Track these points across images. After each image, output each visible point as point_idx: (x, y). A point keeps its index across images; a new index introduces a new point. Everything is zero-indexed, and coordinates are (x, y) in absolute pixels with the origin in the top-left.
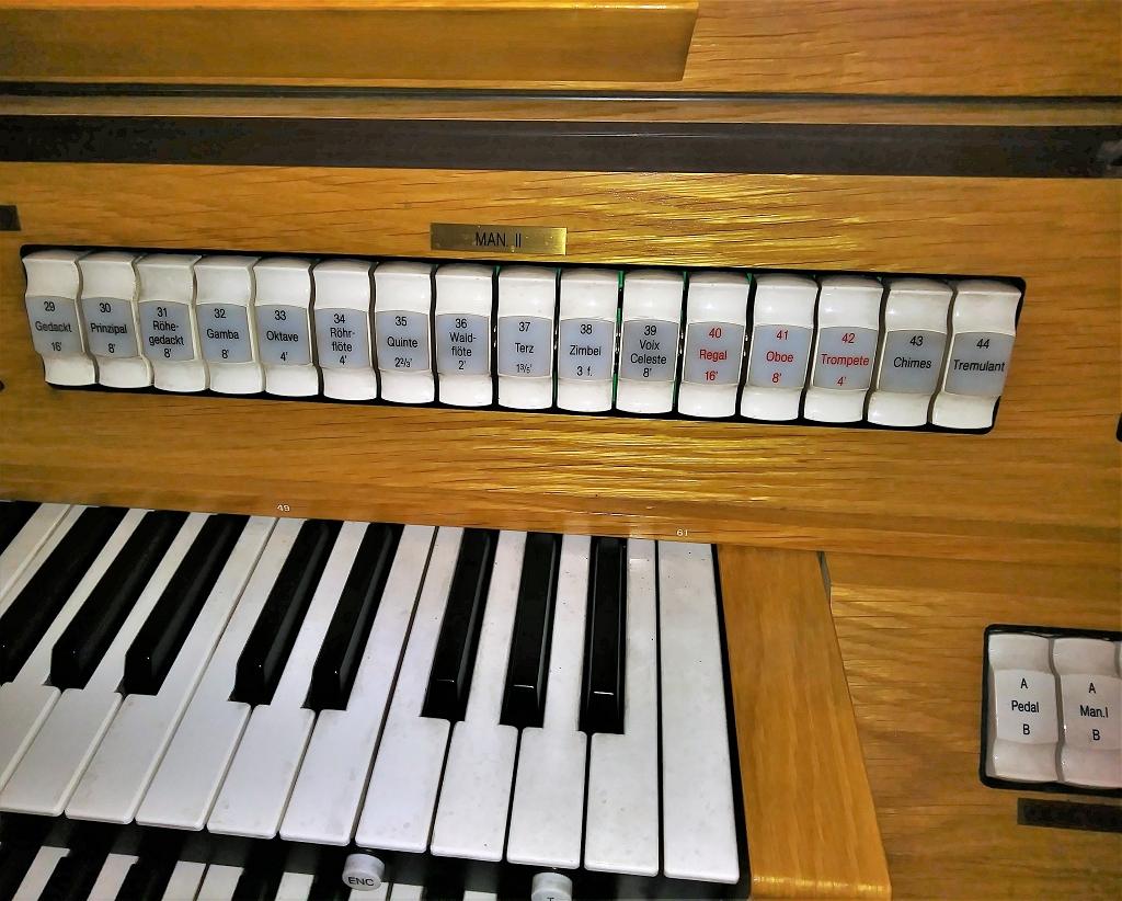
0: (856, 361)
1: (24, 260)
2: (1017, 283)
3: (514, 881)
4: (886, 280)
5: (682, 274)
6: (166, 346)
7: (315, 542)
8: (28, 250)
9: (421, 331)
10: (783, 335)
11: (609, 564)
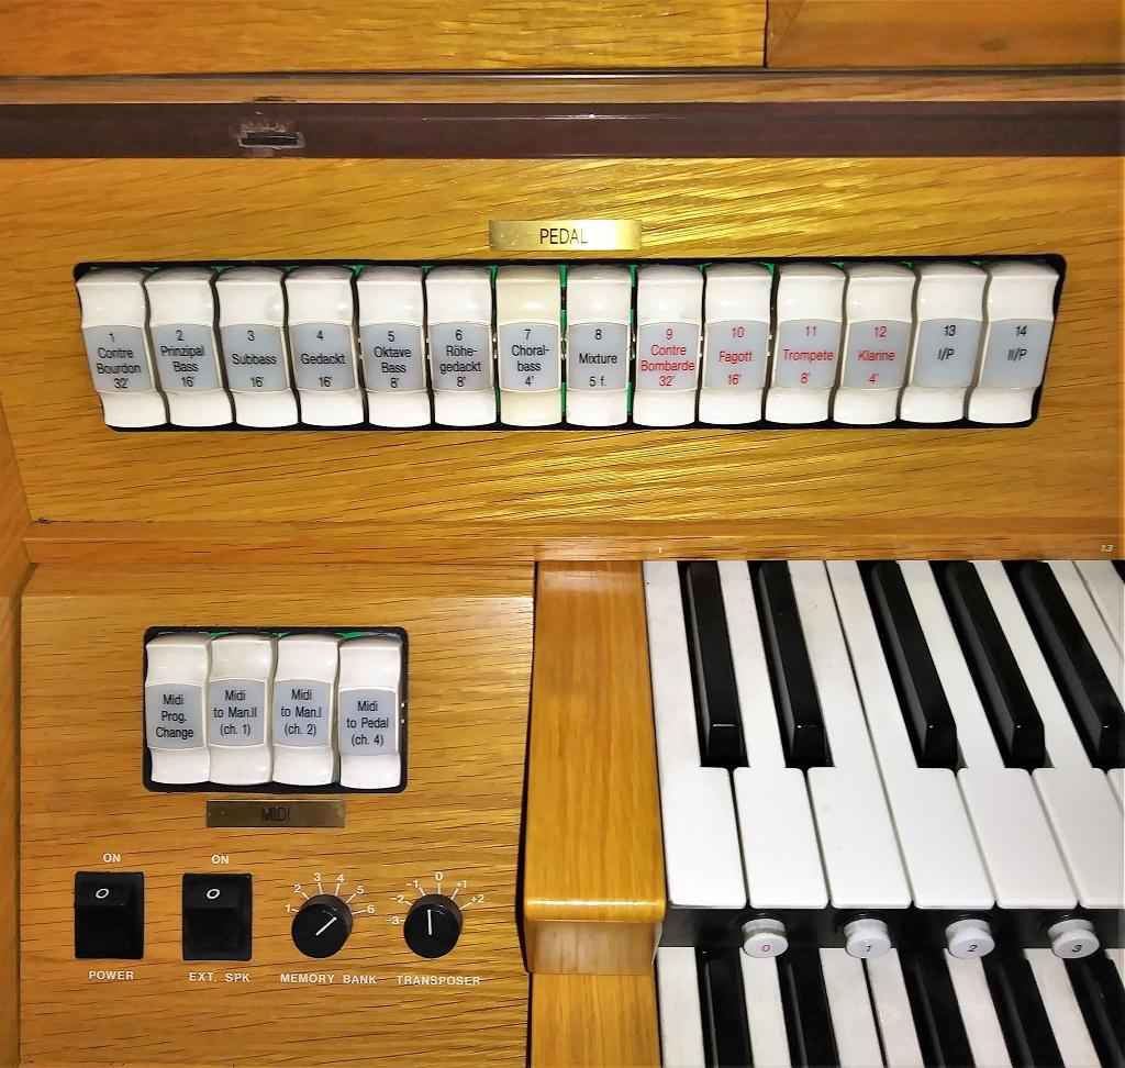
0: (819, 356)
1: (80, 284)
2: (1055, 263)
4: (776, 266)
6: (460, 374)
7: (700, 587)
10: (812, 330)
11: (1034, 582)
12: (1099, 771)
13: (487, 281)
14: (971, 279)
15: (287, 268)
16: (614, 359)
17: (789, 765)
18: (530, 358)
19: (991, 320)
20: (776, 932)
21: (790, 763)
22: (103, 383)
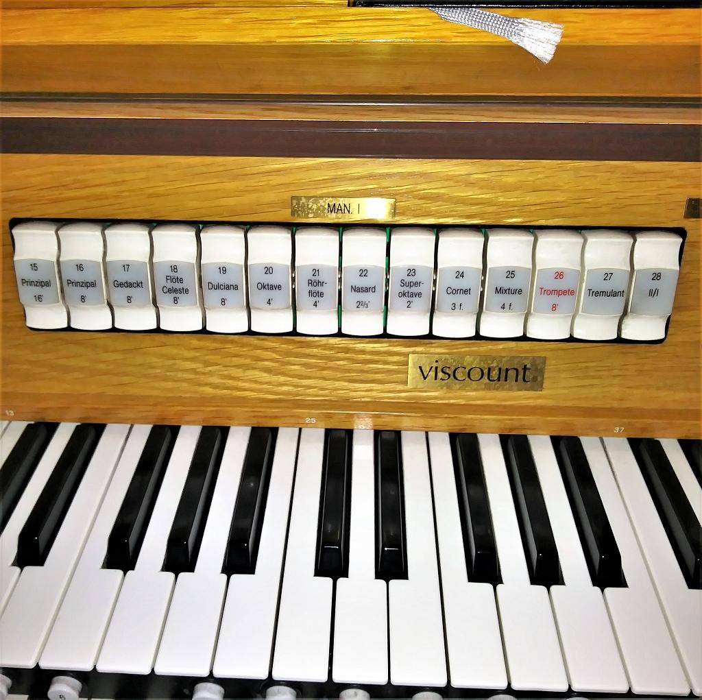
2: (681, 232)
3: (183, 687)
4: (438, 229)
5: (481, 231)
8: (15, 222)
9: (283, 278)
12: (597, 589)
13: (242, 235)
14: (573, 240)
15: (107, 223)
16: (279, 287)
17: (377, 577)
18: (410, 289)
19: (538, 268)
20: (73, 688)
21: (534, 581)
22: (26, 293)
